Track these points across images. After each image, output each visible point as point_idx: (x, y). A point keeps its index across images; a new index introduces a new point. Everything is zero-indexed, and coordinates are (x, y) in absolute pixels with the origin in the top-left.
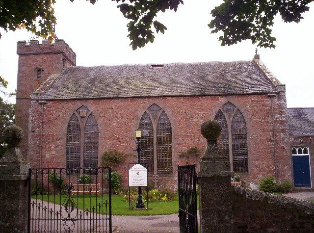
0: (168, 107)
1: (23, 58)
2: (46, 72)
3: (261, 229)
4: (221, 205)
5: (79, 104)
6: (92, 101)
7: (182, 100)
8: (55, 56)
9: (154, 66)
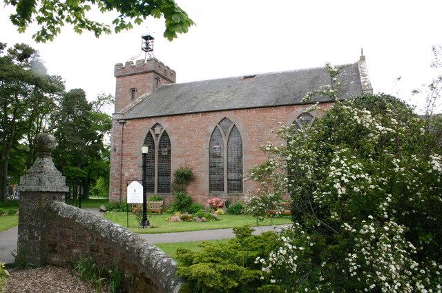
0: (238, 119)
1: (120, 79)
2: (139, 91)
3: (67, 249)
4: (32, 220)
5: (154, 122)
6: (165, 118)
7: (254, 112)
8: (147, 75)
9: (245, 77)
